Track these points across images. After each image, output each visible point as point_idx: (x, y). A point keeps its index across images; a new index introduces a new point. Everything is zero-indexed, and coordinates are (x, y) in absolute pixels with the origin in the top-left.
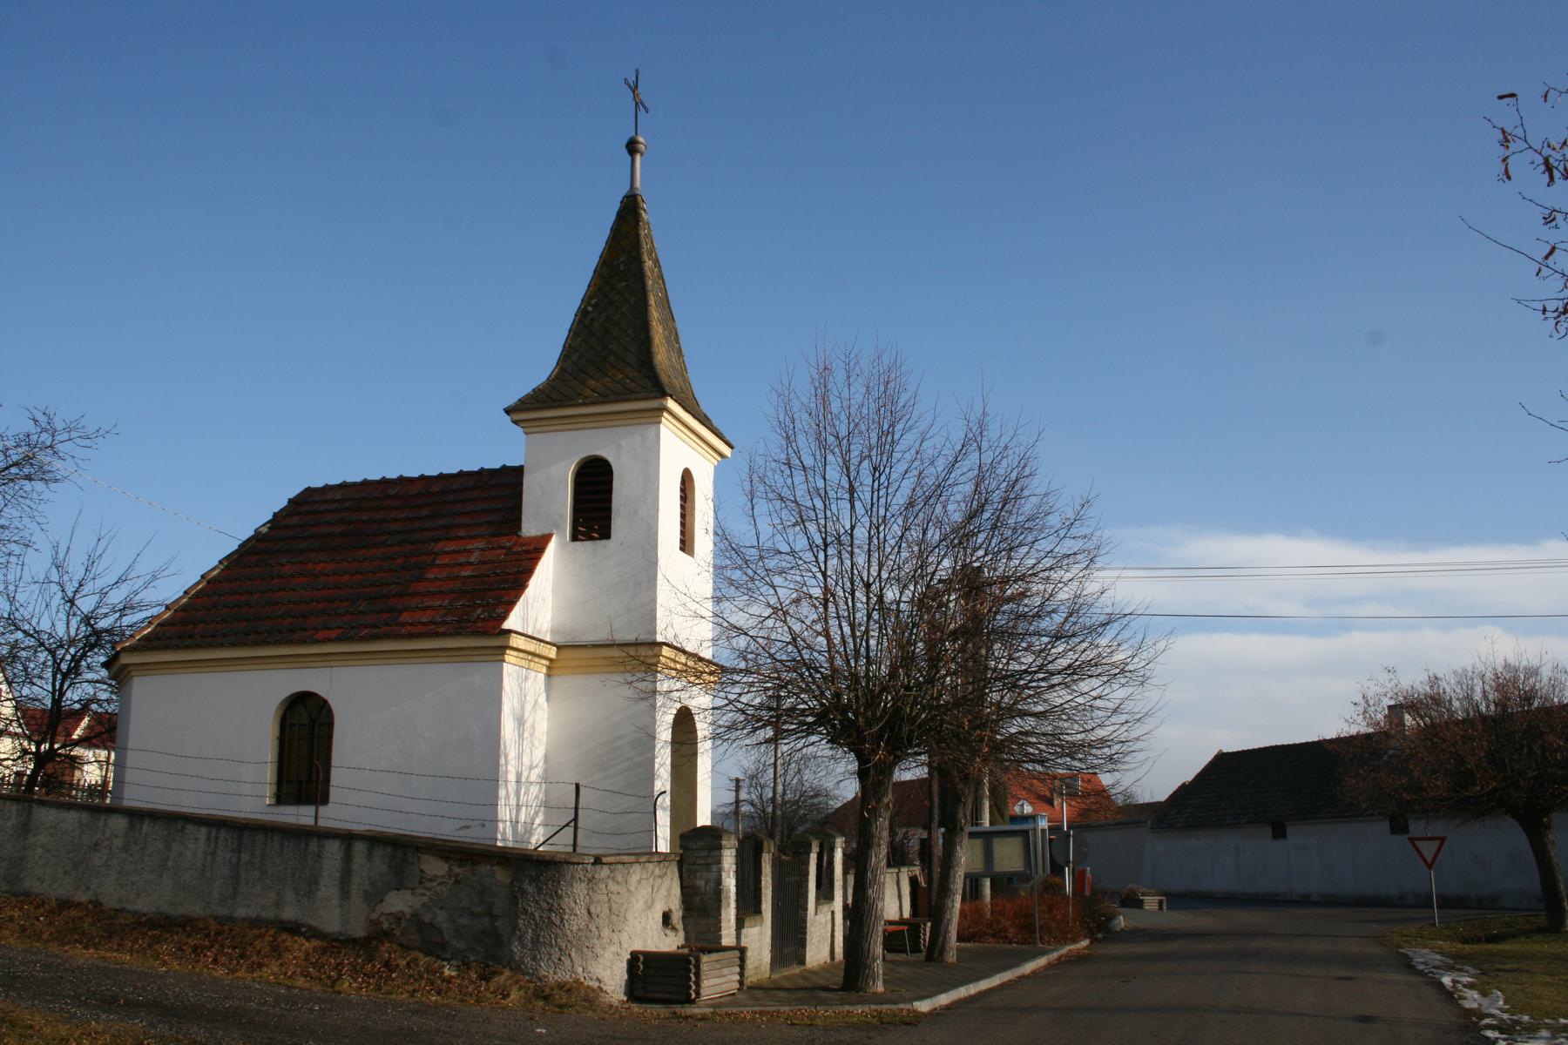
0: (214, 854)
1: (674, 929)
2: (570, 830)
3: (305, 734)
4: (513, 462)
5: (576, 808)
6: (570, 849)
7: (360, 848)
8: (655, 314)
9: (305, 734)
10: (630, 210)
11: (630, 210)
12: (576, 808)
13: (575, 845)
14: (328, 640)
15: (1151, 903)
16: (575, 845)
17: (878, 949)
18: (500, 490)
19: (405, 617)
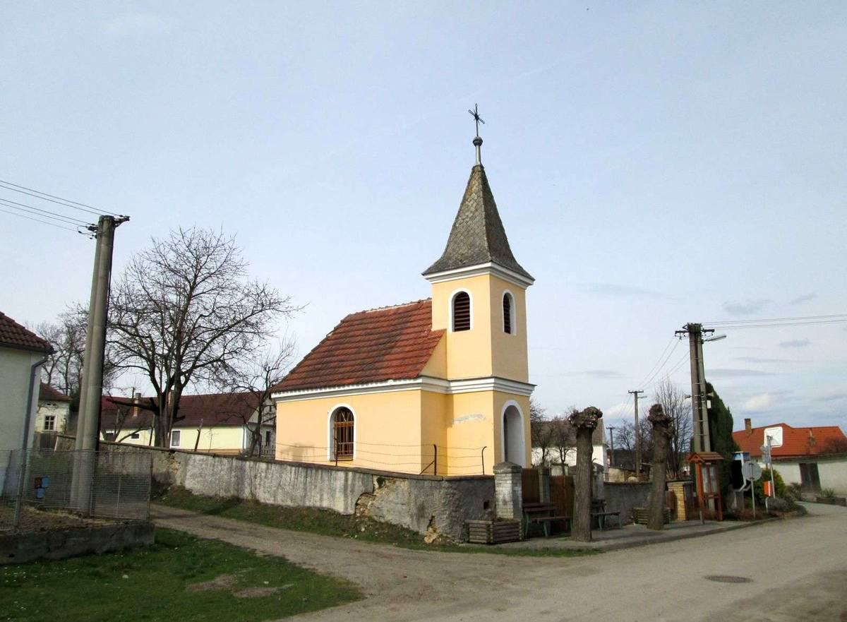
0: (297, 479)
1: (768, 436)
2: (433, 466)
3: (343, 422)
4: (424, 298)
5: (436, 456)
6: (433, 474)
7: (350, 474)
8: (181, 512)
9: (343, 422)
10: (479, 173)
11: (479, 173)
12: (436, 456)
13: (435, 472)
14: (349, 384)
15: (694, 495)
16: (435, 472)
17: (554, 518)
18: (423, 309)
19: (381, 371)
